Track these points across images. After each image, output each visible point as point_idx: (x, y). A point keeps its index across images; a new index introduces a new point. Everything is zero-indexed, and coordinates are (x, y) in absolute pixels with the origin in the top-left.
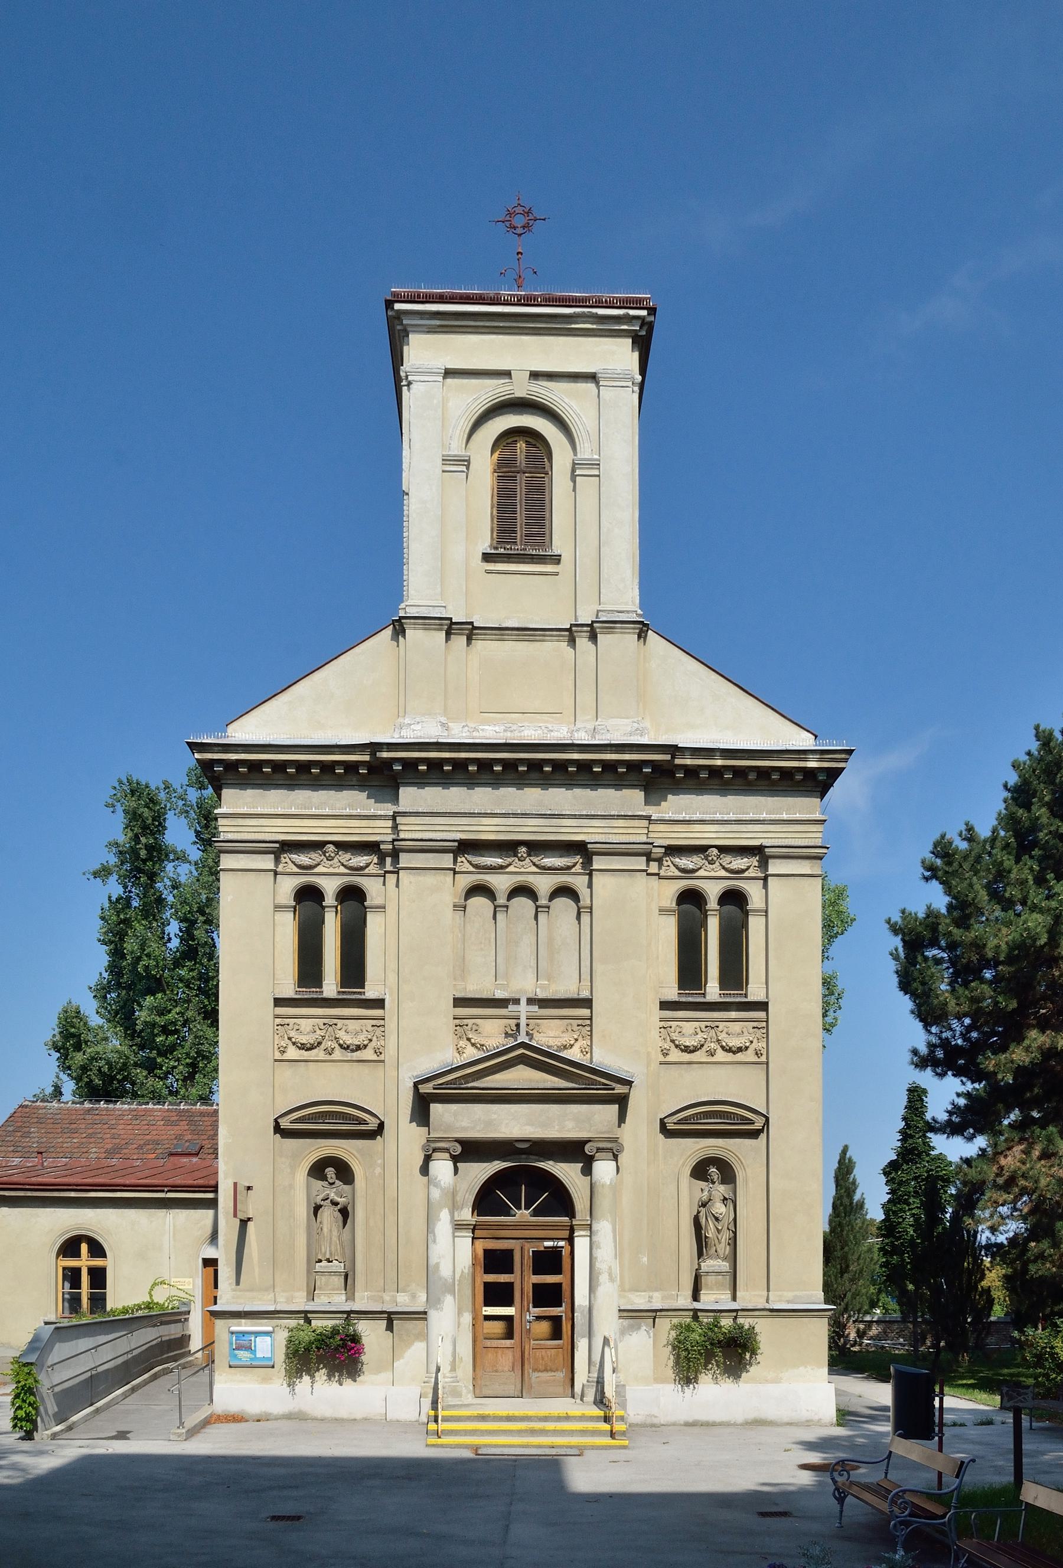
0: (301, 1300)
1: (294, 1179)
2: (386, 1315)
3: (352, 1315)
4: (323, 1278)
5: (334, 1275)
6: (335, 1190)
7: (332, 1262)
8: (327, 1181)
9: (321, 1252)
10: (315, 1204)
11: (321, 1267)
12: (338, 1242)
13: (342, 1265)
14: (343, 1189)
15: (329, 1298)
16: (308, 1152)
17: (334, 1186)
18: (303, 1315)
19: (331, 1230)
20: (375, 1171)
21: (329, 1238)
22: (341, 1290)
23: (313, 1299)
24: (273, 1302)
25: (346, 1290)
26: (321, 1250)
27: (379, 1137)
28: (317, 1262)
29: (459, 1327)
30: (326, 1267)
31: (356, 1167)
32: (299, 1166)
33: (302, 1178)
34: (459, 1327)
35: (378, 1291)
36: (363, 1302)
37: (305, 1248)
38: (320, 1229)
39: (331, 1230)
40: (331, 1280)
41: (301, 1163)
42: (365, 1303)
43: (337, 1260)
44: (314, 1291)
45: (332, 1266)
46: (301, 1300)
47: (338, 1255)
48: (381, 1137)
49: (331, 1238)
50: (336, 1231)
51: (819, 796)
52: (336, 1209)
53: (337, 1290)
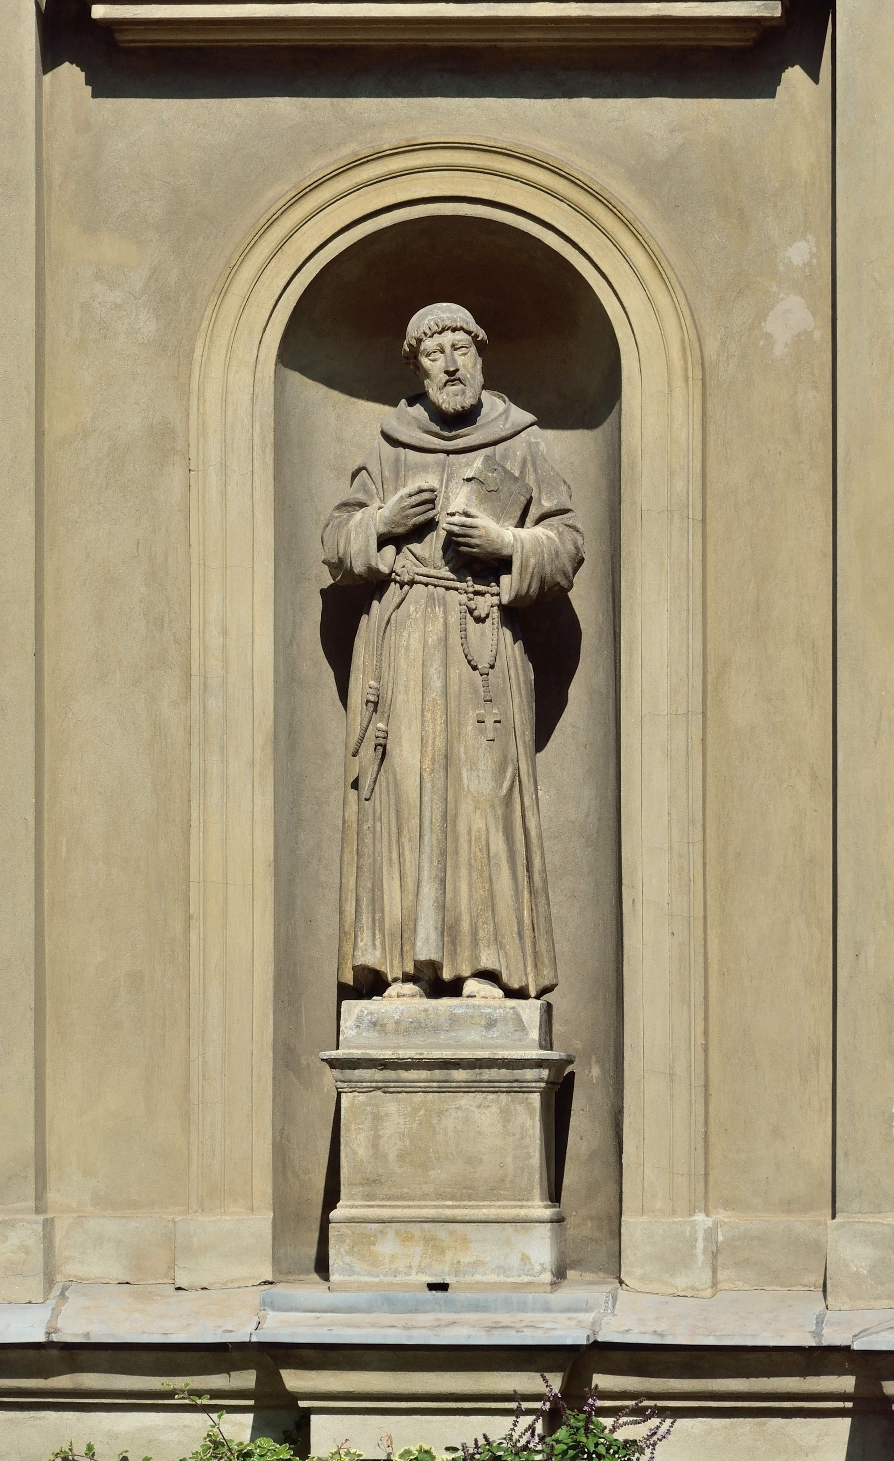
0: (239, 1271)
1: (185, 393)
2: (847, 1383)
3: (602, 1381)
4: (392, 1105)
5: (468, 1088)
6: (475, 463)
7: (454, 988)
8: (419, 397)
9: (377, 923)
10: (338, 566)
11: (376, 1025)
12: (498, 844)
13: (530, 1010)
14: (532, 459)
15: (434, 1245)
16: (286, 188)
17: (471, 436)
18: (246, 1379)
19: (448, 760)
20: (770, 326)
21: (433, 812)
22: (522, 1196)
23: (322, 1267)
24: (36, 1284)
25: (554, 1194)
26: (377, 903)
27: (794, 75)
28: (346, 992)
29: (129, 1284)
30: (417, 1027)
31: (633, 298)
32: (223, 293)
33: (241, 377)
34: (129, 1284)
35: (790, 1205)
36: (681, 1282)
37: (265, 887)
38: (368, 753)
39: (448, 760)
40: (449, 1122)
41: (233, 270)
42: (692, 1293)
43: (490, 976)
44: (332, 1197)
45: (454, 1020)
46: (239, 1271)
47: (497, 940)
48: (814, 74)
49: (448, 819)
50: (486, 763)
51: (550, 1080)
52: (483, 605)
53: (494, 1192)
